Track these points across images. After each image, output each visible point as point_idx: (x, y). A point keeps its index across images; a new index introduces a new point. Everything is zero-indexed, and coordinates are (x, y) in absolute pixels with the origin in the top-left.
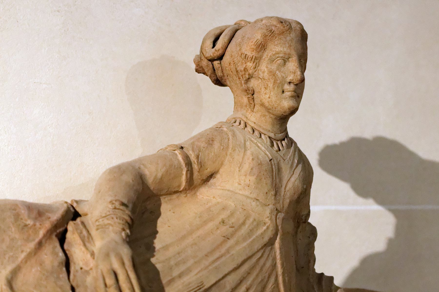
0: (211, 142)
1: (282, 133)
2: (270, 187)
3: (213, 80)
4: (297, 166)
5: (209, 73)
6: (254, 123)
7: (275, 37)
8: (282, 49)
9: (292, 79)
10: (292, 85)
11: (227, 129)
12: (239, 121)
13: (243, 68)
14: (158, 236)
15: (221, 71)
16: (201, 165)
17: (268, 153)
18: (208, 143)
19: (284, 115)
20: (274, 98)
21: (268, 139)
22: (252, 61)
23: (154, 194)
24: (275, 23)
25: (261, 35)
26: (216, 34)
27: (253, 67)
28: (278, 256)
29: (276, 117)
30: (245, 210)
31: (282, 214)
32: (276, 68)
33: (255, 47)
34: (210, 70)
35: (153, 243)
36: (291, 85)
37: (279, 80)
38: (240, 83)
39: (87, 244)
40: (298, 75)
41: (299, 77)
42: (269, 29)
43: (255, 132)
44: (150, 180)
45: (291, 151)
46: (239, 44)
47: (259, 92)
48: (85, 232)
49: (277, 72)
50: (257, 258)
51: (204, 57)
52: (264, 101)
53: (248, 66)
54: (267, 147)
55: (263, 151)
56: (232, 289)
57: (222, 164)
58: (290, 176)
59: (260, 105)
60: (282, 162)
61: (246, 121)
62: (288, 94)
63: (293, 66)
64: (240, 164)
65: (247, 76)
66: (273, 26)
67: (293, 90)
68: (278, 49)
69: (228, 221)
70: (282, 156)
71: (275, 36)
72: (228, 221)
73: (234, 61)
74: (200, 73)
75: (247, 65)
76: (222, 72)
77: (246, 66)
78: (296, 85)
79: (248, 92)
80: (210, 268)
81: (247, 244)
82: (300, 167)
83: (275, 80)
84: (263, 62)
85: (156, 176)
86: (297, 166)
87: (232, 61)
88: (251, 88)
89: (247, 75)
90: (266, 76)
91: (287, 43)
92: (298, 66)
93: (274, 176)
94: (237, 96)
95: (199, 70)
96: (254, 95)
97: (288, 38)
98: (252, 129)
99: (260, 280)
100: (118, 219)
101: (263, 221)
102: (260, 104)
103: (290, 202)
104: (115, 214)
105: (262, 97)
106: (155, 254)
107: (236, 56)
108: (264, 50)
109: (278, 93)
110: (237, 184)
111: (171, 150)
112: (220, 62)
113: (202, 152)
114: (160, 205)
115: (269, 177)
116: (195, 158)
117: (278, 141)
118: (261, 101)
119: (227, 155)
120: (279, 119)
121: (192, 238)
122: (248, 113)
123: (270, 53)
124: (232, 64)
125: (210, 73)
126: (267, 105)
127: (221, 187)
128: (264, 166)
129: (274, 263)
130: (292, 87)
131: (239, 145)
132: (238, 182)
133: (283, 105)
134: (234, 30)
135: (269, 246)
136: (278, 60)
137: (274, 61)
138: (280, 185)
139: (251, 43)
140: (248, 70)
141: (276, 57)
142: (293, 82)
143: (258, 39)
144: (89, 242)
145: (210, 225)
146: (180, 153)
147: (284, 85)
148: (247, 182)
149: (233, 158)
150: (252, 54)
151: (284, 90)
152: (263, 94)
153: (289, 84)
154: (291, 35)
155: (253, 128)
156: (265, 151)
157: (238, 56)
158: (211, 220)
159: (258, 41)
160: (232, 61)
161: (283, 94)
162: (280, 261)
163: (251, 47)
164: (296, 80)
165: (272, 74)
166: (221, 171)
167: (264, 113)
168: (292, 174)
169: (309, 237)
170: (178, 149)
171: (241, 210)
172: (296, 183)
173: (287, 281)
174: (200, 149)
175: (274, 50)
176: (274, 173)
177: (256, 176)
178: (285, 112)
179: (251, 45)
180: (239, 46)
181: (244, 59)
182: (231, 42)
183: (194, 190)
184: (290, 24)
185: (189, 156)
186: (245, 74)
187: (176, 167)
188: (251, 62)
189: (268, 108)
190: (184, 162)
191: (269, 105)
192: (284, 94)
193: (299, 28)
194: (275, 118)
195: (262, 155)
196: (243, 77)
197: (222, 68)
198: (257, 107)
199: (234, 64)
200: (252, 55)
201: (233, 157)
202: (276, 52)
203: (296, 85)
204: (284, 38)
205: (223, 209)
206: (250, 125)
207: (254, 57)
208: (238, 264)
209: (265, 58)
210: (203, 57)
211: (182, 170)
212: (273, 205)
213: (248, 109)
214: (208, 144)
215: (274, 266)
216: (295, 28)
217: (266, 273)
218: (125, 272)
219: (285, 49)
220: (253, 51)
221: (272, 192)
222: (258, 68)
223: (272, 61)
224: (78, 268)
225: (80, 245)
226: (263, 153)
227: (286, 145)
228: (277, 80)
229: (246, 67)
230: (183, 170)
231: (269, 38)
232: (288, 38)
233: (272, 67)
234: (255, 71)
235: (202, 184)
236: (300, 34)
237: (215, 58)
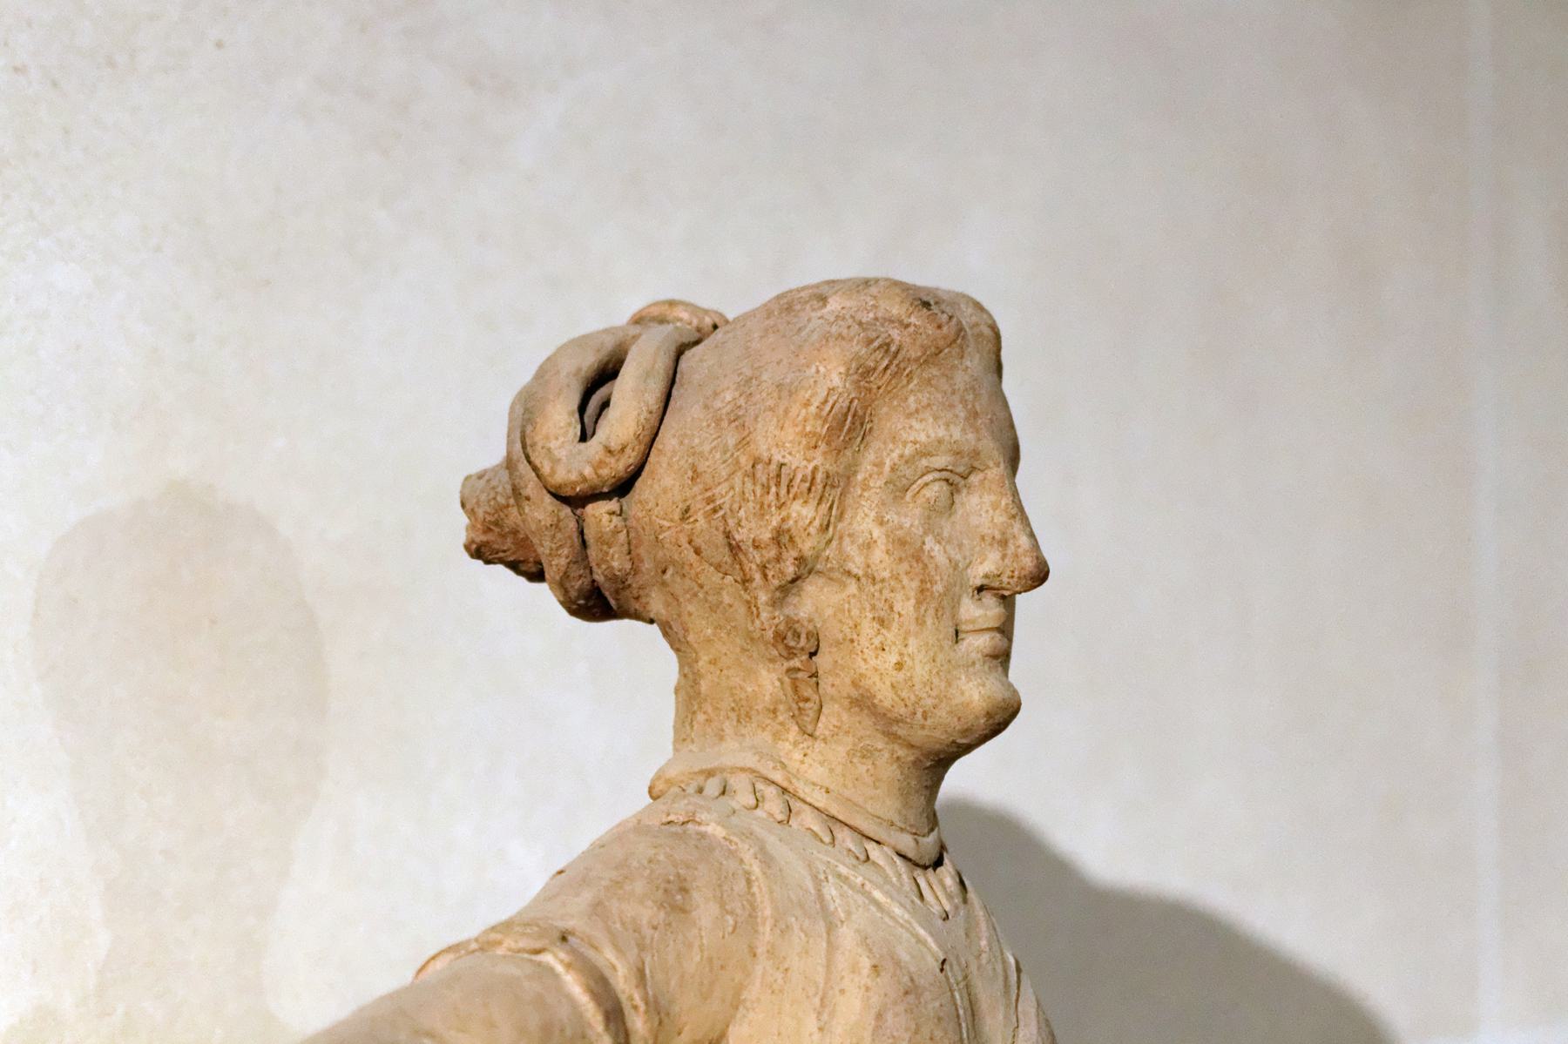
0: (679, 897)
6: (823, 790)
7: (907, 375)
8: (941, 433)
13: (770, 528)
16: (658, 1011)
17: (922, 932)
18: (665, 905)
20: (923, 668)
22: (811, 495)
25: (842, 369)
26: (583, 373)
27: (817, 523)
29: (917, 758)
32: (920, 523)
33: (823, 426)
34: (568, 545)
36: (984, 600)
37: (942, 579)
40: (1020, 550)
42: (877, 337)
49: (930, 543)
53: (796, 522)
57: (736, 1004)
63: (991, 511)
65: (790, 570)
66: (893, 322)
67: (996, 625)
68: (924, 431)
71: (904, 369)
73: (710, 500)
75: (789, 517)
77: (783, 520)
79: (792, 644)
83: (922, 581)
88: (806, 623)
89: (788, 563)
90: (883, 566)
97: (961, 379)
105: (862, 663)
108: (859, 439)
109: (938, 640)
111: (519, 951)
112: (618, 504)
118: (855, 684)
119: (755, 955)
120: (928, 764)
124: (699, 514)
126: (887, 704)
136: (927, 484)
137: (907, 490)
140: (797, 539)
141: (919, 473)
142: (996, 584)
146: (568, 966)
150: (809, 461)
153: (977, 597)
154: (968, 363)
156: (910, 923)
159: (835, 398)
160: (699, 497)
161: (956, 647)
165: (909, 551)
167: (868, 742)
179: (800, 418)
180: (733, 425)
185: (607, 973)
186: (778, 559)
187: (568, 1032)
189: (889, 715)
191: (896, 699)
192: (963, 646)
194: (916, 763)
196: (770, 574)
198: (834, 715)
199: (715, 511)
200: (811, 467)
201: (786, 966)
202: (918, 446)
204: (943, 380)
207: (820, 476)
213: (781, 724)
214: (669, 909)
219: (957, 433)
223: (899, 489)
226: (906, 935)
228: (933, 583)
229: (785, 527)
231: (880, 384)
232: (961, 379)
233: (903, 520)
237: (603, 487)
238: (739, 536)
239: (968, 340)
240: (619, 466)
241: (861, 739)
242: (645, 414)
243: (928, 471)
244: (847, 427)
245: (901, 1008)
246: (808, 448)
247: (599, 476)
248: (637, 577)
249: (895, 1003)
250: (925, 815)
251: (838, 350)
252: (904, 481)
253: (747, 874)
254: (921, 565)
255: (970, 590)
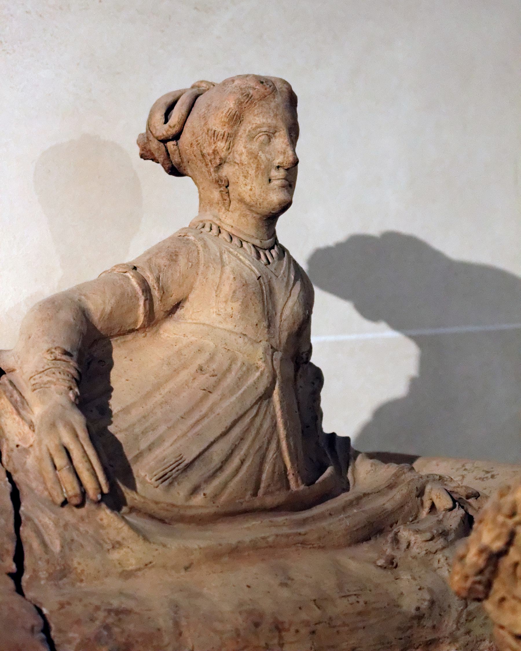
1: (270, 238)
2: (261, 316)
3: (167, 169)
4: (294, 285)
5: (161, 159)
6: (231, 227)
8: (264, 121)
9: (282, 162)
10: (282, 171)
11: (194, 237)
12: (210, 226)
13: (212, 150)
14: (113, 394)
15: (179, 155)
16: (163, 290)
17: (254, 268)
19: (273, 213)
21: (252, 247)
22: (224, 139)
23: (103, 335)
24: (252, 84)
25: (234, 102)
26: (168, 103)
27: (225, 148)
28: (278, 413)
30: (229, 350)
31: (279, 352)
35: (108, 404)
38: (208, 171)
39: (23, 412)
40: (289, 155)
41: (291, 159)
42: (245, 93)
43: (233, 239)
44: (96, 317)
45: (285, 263)
46: (203, 115)
47: (235, 182)
48: (16, 396)
49: (260, 153)
50: (250, 417)
51: (154, 137)
52: (244, 195)
54: (251, 260)
55: (248, 267)
56: (222, 462)
57: (192, 288)
58: (287, 299)
59: (239, 200)
60: (274, 280)
61: (219, 225)
62: (276, 183)
64: (217, 286)
65: (218, 161)
67: (283, 178)
69: (207, 368)
70: (273, 271)
71: (253, 102)
72: (207, 368)
73: (197, 141)
74: (148, 159)
75: (217, 146)
76: (180, 156)
77: (216, 147)
78: (287, 170)
79: (220, 183)
80: (190, 435)
81: (237, 398)
82: (298, 284)
83: (257, 165)
84: (239, 140)
85: (104, 309)
86: (294, 285)
87: (195, 140)
88: (224, 177)
89: (218, 160)
91: (271, 111)
92: (288, 144)
93: (265, 300)
94: (203, 189)
95: (145, 155)
96: (228, 188)
97: (273, 104)
98: (229, 235)
99: (258, 447)
100: (62, 373)
101: (254, 364)
102: (238, 199)
103: (289, 335)
104: (56, 368)
106: (112, 419)
107: (201, 133)
108: (239, 123)
110: (214, 315)
113: (163, 272)
114: (110, 352)
115: (259, 302)
116: (155, 281)
117: (265, 250)
118: (239, 195)
119: (198, 274)
121: (161, 394)
122: (221, 213)
123: (248, 127)
125: (162, 159)
127: (193, 320)
128: (251, 286)
129: (275, 421)
130: (281, 173)
131: (214, 259)
132: (216, 312)
133: (271, 200)
134: (193, 97)
135: (266, 399)
136: (260, 136)
138: (274, 313)
139: (221, 115)
140: (220, 153)
141: (258, 133)
143: (231, 108)
144: (24, 409)
145: (184, 375)
146: (133, 276)
147: (270, 171)
148: (229, 310)
149: (207, 279)
150: (223, 129)
151: (271, 178)
152: (241, 186)
154: (277, 100)
155: (231, 235)
156: (250, 266)
157: (202, 133)
158: (184, 367)
159: (231, 111)
160: (195, 140)
161: (269, 184)
162: (281, 419)
163: (221, 120)
164: (287, 163)
165: (254, 156)
166: (191, 297)
168: (289, 296)
169: (313, 383)
170: (129, 270)
171: (224, 351)
172: (295, 308)
173: (293, 447)
174: (160, 267)
175: (253, 122)
176: (265, 295)
177: (241, 302)
178: (273, 209)
179: (220, 117)
180: (204, 119)
181: (213, 138)
182: (191, 114)
183: (156, 326)
184: (273, 84)
186: (214, 158)
188: (222, 142)
189: (249, 204)
190: (141, 287)
192: (272, 184)
193: (286, 88)
194: (260, 218)
195: (246, 271)
196: (213, 163)
197: (179, 150)
198: (234, 204)
199: (198, 144)
200: (223, 131)
201: (207, 277)
202: (257, 125)
203: (287, 170)
204: (267, 105)
205: (199, 350)
206: (226, 231)
207: (226, 134)
208: (226, 427)
209: (242, 134)
210: (152, 136)
211: (138, 299)
212: (267, 341)
213: (220, 207)
214: (170, 261)
215: (275, 426)
216: (281, 90)
217: (265, 437)
218: (80, 446)
219: (269, 121)
220: (225, 125)
221: (264, 323)
222: (233, 149)
223: (251, 138)
224: (13, 446)
225: (12, 413)
227: (276, 256)
229: (216, 149)
230: (140, 299)
232: (273, 104)
234: (230, 153)
235: (166, 317)
236: (288, 97)
237: (170, 137)
238: (205, 151)
239: (278, 93)
240: (173, 131)
241: (242, 211)
242: (181, 116)
243: (260, 132)
244: (234, 119)
245: (241, 290)
246: (222, 126)
247: (167, 134)
248: (184, 164)
249: (239, 288)
250: (266, 234)
251: (233, 97)
252: (253, 135)
253: (198, 250)
254: (257, 160)
255: (275, 167)
